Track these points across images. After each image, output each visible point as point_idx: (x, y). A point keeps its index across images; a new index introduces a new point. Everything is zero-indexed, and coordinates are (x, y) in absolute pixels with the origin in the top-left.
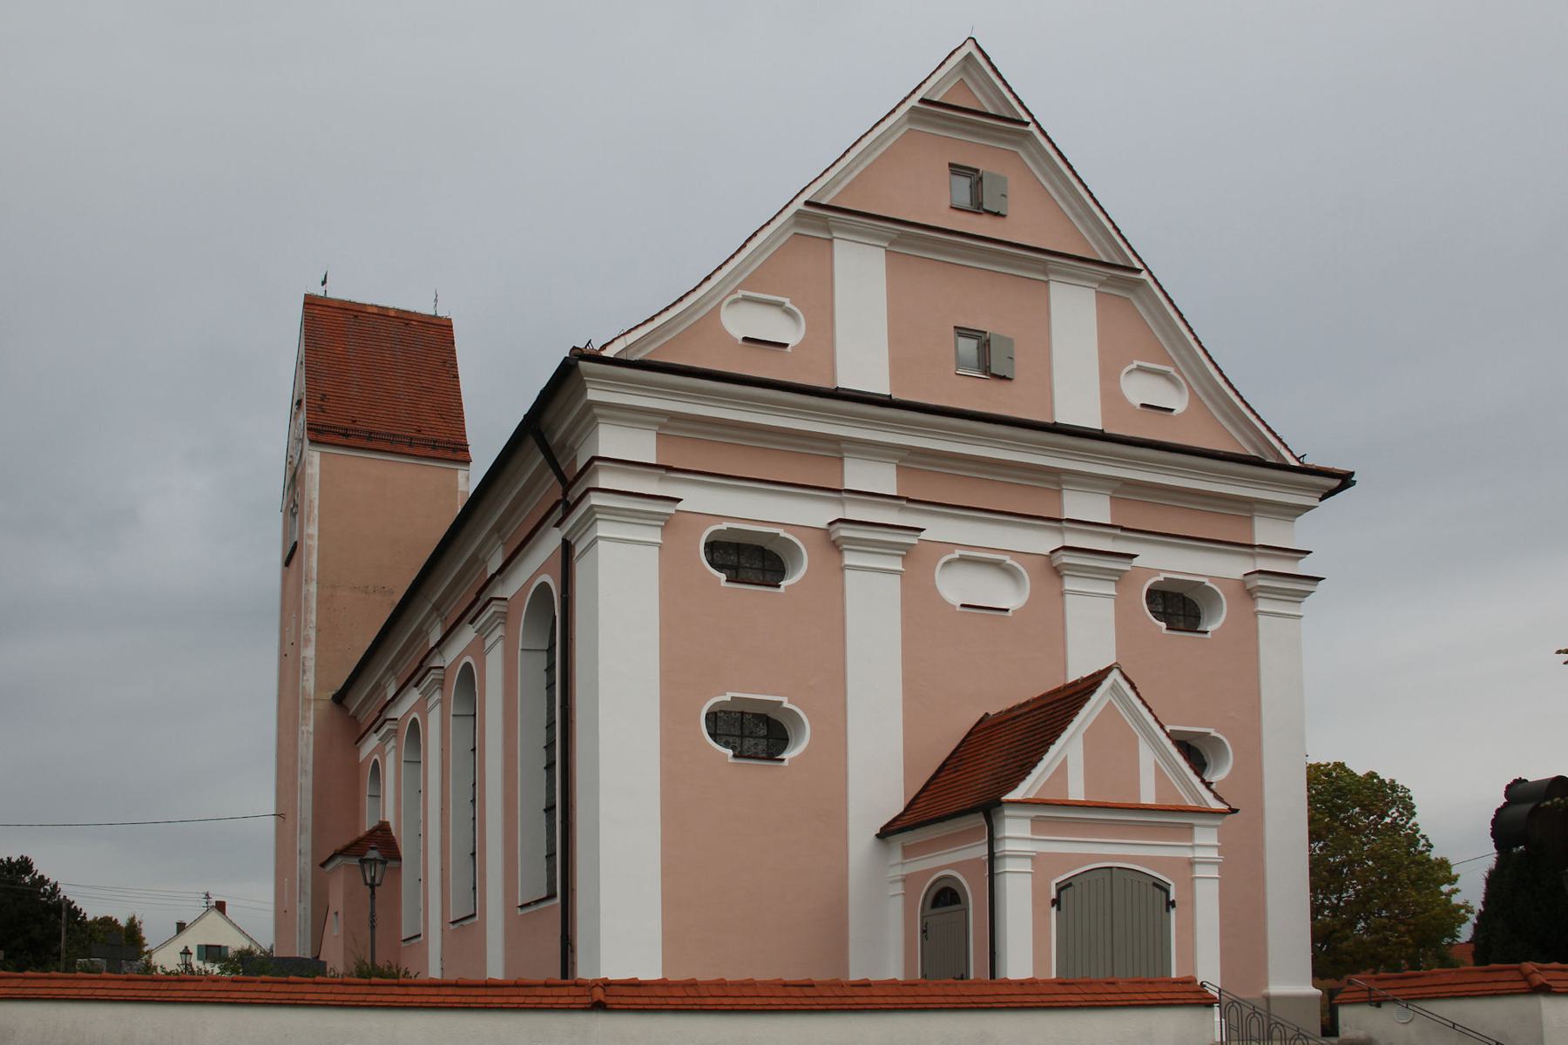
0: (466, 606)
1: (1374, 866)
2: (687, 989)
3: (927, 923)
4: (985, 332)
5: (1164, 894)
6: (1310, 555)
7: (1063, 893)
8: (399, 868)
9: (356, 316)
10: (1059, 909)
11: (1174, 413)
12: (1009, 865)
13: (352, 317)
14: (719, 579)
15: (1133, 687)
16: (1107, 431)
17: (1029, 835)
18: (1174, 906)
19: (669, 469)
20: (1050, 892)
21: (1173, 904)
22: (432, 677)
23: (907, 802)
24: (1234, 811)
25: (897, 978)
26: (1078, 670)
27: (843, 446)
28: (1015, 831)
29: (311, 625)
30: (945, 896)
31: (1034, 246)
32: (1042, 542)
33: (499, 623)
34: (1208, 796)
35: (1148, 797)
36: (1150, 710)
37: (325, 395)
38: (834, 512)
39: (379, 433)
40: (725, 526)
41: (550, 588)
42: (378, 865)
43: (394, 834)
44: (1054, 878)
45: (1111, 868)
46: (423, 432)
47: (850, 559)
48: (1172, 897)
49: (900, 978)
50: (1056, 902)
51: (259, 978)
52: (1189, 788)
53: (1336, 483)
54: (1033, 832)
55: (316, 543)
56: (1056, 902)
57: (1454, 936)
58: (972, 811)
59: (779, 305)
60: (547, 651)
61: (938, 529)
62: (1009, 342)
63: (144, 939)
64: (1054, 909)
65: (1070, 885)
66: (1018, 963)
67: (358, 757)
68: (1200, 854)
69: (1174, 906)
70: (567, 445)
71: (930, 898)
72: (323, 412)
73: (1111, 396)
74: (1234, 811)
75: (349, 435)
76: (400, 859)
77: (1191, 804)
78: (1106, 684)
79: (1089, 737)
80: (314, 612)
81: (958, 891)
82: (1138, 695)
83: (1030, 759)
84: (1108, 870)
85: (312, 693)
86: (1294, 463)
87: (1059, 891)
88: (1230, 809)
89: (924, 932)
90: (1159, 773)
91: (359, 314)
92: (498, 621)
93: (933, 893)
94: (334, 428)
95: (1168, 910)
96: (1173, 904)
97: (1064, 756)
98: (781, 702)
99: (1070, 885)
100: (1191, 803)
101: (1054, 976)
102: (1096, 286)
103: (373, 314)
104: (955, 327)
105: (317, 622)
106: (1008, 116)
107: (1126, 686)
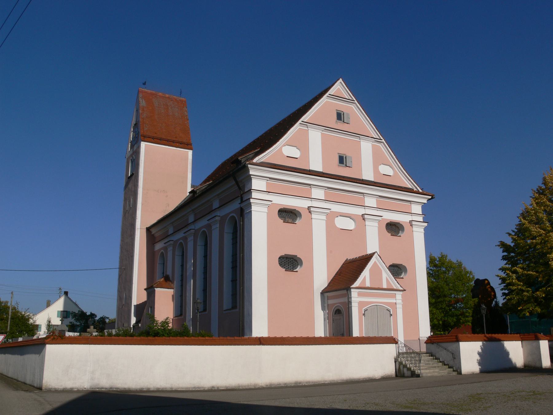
0: (210, 218)
1: (539, 280)
5: (388, 312)
7: (366, 312)
10: (365, 316)
15: (380, 258)
18: (392, 316)
20: (362, 312)
21: (391, 315)
23: (329, 282)
24: (404, 290)
25: (507, 243)
26: (369, 252)
27: (311, 186)
28: (354, 293)
32: (359, 211)
34: (399, 286)
35: (385, 286)
36: (385, 264)
41: (235, 217)
44: (364, 308)
48: (391, 313)
49: (323, 336)
50: (364, 314)
52: (394, 284)
56: (364, 314)
57: (436, 324)
58: (344, 289)
61: (336, 208)
62: (351, 158)
63: (60, 320)
64: (364, 316)
65: (367, 310)
66: (356, 333)
69: (392, 316)
73: (376, 170)
77: (395, 288)
78: (374, 257)
79: (371, 270)
82: (381, 259)
84: (376, 306)
87: (365, 312)
88: (404, 290)
90: (387, 279)
93: (335, 310)
95: (390, 317)
96: (391, 315)
97: (364, 276)
99: (367, 310)
100: (395, 288)
101: (405, 351)
102: (371, 143)
104: (336, 110)
107: (379, 257)
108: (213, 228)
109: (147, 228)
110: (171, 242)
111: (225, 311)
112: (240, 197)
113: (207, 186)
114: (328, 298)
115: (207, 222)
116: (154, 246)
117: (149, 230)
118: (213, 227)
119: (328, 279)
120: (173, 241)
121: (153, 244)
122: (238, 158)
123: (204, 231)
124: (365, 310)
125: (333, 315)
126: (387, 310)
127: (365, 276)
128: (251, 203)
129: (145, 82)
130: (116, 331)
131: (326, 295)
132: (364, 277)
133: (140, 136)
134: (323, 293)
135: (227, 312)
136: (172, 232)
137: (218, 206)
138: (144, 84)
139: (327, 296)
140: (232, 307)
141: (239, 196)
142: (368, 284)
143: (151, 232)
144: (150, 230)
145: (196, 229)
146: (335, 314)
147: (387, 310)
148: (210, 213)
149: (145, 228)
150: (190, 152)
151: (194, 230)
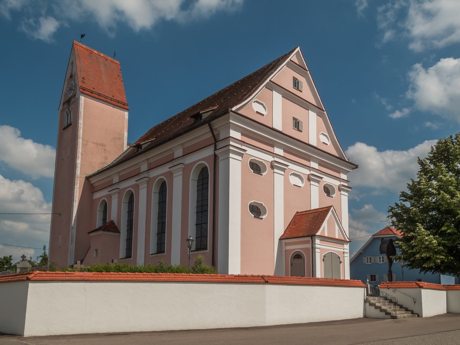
2: (221, 277)
3: (292, 262)
4: (298, 119)
6: (349, 182)
7: (324, 258)
8: (119, 236)
9: (91, 53)
10: (324, 262)
11: (328, 145)
12: (317, 250)
13: (90, 53)
14: (252, 171)
16: (317, 147)
17: (319, 244)
19: (244, 142)
21: (341, 262)
22: (145, 180)
24: (351, 241)
29: (80, 153)
30: (298, 256)
31: (296, 94)
33: (182, 170)
37: (84, 78)
38: (273, 159)
39: (102, 94)
40: (253, 158)
42: (190, 241)
43: (116, 225)
45: (332, 253)
46: (114, 97)
47: (276, 170)
51: (398, 282)
53: (355, 167)
54: (320, 243)
55: (82, 126)
59: (262, 104)
60: (197, 181)
64: (323, 262)
65: (325, 256)
66: (319, 274)
67: (92, 197)
68: (345, 251)
70: (218, 130)
71: (293, 257)
72: (84, 83)
73: (318, 139)
74: (351, 241)
75: (93, 93)
76: (120, 233)
79: (328, 221)
80: (81, 148)
81: (301, 255)
83: (319, 225)
85: (79, 175)
86: (347, 160)
87: (324, 257)
89: (291, 264)
91: (92, 52)
92: (181, 170)
94: (88, 89)
98: (262, 204)
99: (325, 256)
103: (96, 54)
105: (81, 152)
106: (304, 68)
107: (334, 211)
108: (112, 198)
109: (86, 177)
110: (181, 166)
111: (120, 259)
112: (214, 145)
113: (149, 143)
114: (286, 244)
115: (108, 193)
116: (93, 194)
117: (88, 178)
118: (113, 197)
119: (284, 229)
120: (184, 165)
121: (92, 193)
122: (199, 112)
123: (104, 200)
124: (324, 256)
125: (291, 259)
126: (338, 257)
127: (324, 226)
128: (172, 171)
129: (82, 37)
130: (201, 259)
131: (284, 241)
132: (323, 227)
133: (78, 88)
134: (281, 239)
135: (121, 260)
136: (118, 182)
137: (181, 155)
138: (82, 36)
139: (285, 243)
140: (196, 249)
141: (212, 144)
142: (326, 235)
143: (90, 181)
144: (90, 179)
145: (150, 177)
146: (294, 258)
147: (338, 257)
148: (171, 161)
149: (85, 177)
150: (126, 114)
151: (148, 178)
